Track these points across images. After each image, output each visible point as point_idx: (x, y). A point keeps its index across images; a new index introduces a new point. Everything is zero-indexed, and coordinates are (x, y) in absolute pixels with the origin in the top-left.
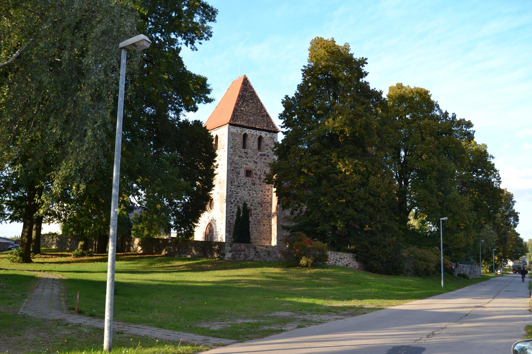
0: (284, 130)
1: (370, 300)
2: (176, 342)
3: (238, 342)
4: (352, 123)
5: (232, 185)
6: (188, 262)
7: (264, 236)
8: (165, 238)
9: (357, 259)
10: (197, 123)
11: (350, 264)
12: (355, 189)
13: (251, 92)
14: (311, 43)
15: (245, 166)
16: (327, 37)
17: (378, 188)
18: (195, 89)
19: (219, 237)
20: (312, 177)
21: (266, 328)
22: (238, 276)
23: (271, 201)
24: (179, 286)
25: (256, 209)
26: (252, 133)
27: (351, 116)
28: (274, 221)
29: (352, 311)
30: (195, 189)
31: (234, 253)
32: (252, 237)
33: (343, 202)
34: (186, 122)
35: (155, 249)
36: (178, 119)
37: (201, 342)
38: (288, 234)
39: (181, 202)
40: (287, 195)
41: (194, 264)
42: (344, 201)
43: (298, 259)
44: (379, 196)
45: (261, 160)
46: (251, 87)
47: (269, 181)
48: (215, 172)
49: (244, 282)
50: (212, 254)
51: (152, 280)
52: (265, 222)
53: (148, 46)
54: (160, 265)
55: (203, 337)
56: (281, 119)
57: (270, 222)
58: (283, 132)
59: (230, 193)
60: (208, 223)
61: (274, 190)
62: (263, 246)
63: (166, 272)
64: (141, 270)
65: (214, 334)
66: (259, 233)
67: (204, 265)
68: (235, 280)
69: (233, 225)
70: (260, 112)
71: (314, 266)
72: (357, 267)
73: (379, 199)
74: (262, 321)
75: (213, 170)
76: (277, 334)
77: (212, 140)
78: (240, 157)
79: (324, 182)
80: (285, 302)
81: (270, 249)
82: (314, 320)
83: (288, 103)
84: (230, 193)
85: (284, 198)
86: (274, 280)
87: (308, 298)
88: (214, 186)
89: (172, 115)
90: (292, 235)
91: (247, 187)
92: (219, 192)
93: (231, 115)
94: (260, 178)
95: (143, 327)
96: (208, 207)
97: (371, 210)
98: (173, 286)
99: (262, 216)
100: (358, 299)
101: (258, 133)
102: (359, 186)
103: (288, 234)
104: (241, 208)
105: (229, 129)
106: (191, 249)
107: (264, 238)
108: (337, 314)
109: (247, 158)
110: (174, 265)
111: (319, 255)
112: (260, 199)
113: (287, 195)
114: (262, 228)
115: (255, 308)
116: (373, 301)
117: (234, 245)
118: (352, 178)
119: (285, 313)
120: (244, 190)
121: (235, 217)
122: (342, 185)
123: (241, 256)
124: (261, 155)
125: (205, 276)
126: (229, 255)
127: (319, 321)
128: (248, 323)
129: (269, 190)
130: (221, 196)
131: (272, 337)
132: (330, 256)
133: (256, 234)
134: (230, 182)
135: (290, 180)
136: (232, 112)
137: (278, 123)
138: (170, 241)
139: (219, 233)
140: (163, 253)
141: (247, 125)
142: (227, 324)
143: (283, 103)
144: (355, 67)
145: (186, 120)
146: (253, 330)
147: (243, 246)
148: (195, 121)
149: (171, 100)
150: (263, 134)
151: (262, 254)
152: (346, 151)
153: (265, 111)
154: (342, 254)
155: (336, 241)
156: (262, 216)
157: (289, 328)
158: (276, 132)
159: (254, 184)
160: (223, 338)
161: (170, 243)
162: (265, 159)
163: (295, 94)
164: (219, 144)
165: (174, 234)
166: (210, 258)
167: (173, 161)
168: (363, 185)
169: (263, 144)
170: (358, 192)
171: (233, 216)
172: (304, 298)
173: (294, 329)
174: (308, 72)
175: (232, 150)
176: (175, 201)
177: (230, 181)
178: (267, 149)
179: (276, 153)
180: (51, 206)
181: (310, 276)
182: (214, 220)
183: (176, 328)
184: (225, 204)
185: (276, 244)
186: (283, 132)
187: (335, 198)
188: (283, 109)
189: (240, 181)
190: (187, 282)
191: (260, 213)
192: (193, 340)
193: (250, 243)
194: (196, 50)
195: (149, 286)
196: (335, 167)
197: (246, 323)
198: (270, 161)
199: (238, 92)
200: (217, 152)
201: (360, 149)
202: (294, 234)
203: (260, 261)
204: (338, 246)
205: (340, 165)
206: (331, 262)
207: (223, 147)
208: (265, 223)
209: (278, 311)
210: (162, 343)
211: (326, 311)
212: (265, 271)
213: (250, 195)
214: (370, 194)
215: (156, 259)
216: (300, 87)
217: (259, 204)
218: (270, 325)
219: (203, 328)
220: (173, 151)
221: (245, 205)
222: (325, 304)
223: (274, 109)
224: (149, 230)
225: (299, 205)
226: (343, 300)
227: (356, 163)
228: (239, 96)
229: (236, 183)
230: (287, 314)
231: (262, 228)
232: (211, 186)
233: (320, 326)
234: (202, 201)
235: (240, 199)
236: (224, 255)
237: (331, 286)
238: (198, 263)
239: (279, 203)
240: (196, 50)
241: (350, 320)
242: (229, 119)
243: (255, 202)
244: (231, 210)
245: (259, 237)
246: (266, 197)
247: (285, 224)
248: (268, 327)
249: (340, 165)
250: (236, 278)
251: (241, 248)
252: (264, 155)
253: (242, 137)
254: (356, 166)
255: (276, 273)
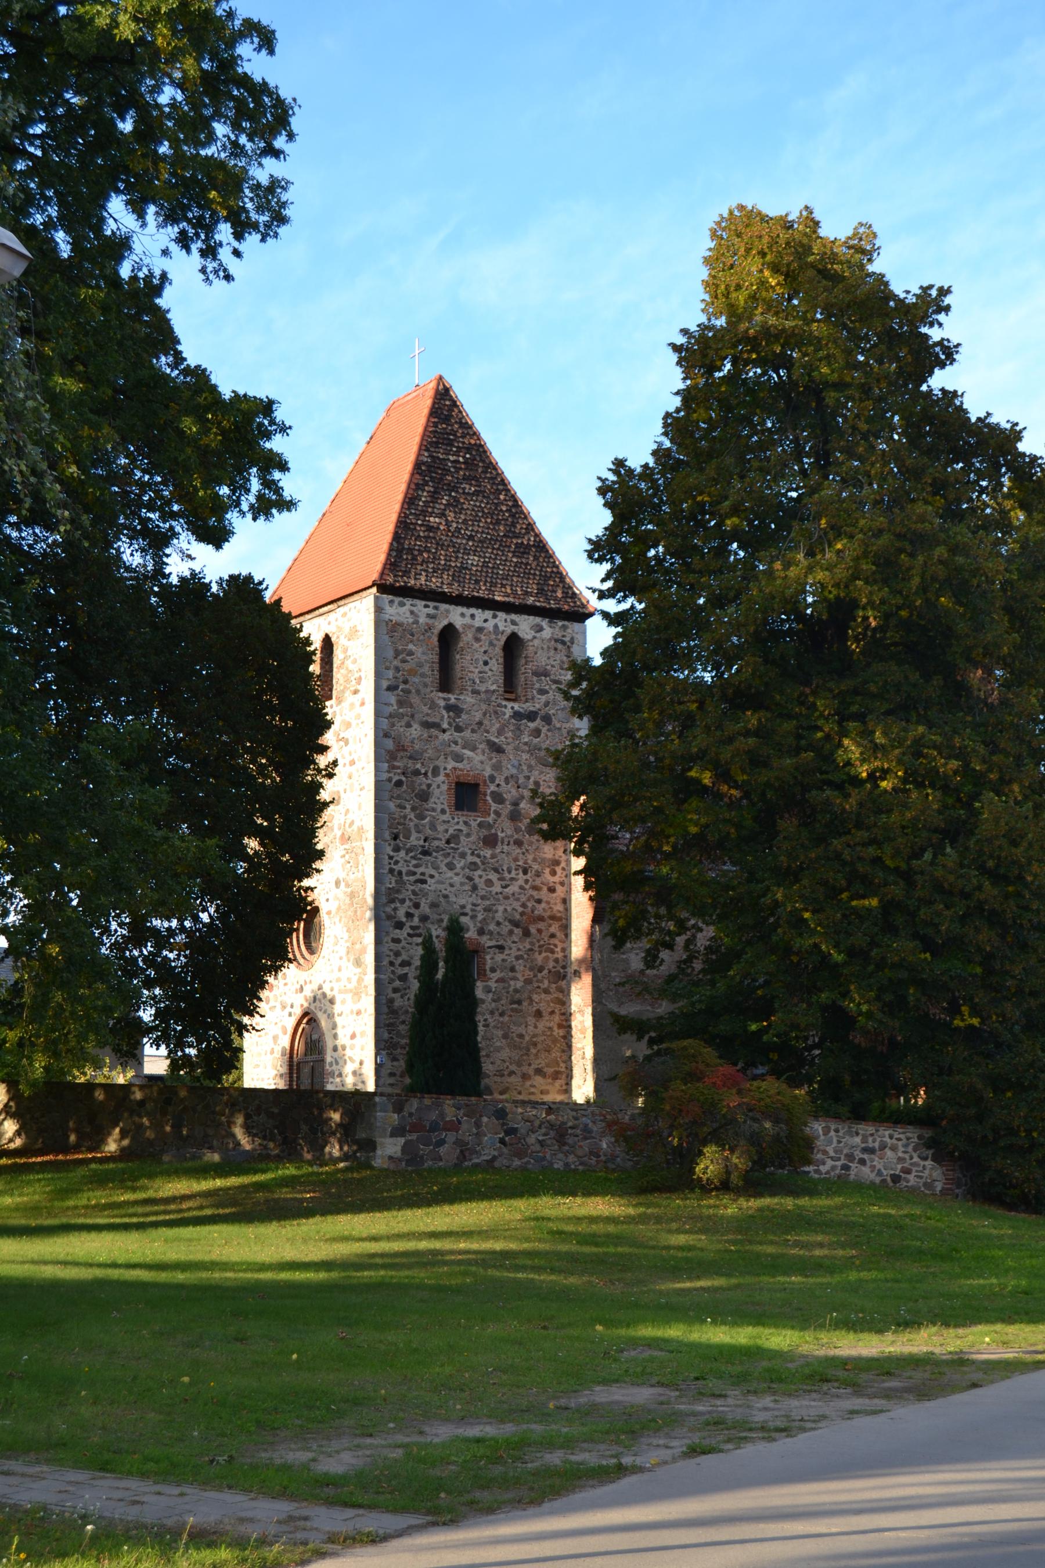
0: (611, 606)
1: (999, 1327)
2: (169, 1531)
3: (434, 1524)
4: (887, 570)
5: (397, 849)
6: (219, 1183)
7: (541, 1062)
8: (121, 1080)
9: (937, 1149)
10: (243, 588)
11: (908, 1171)
12: (917, 854)
13: (468, 450)
14: (714, 234)
15: (451, 764)
16: (780, 203)
17: (1014, 843)
18: (226, 449)
19: (349, 1069)
20: (732, 804)
21: (555, 1458)
22: (434, 1235)
23: (567, 910)
24: (181, 1286)
25: (501, 948)
26: (478, 622)
27: (884, 540)
28: (580, 997)
29: (919, 1376)
30: (241, 867)
31: (414, 1136)
32: (487, 1067)
33: (869, 910)
34: (194, 585)
35: (77, 1131)
36: (159, 571)
37: (272, 1530)
38: (643, 1049)
39: (182, 929)
40: (633, 883)
41: (242, 1188)
42: (874, 902)
43: (688, 1157)
44: (1020, 878)
45: (517, 737)
46: (467, 428)
47: (554, 825)
48: (324, 795)
49: (459, 1263)
50: (318, 1147)
51: (65, 1263)
52: (542, 1001)
53: (17, 269)
54: (100, 1196)
55: (284, 1507)
56: (600, 560)
57: (564, 1002)
58: (606, 615)
59: (391, 882)
60: (298, 1012)
61: (579, 863)
62: (535, 1104)
63: (126, 1227)
64: (19, 1221)
65: (330, 1491)
66: (514, 1046)
67: (285, 1194)
68: (416, 1253)
69: (408, 1018)
70: (511, 534)
71: (753, 1184)
72: (939, 1186)
73: (1019, 895)
74: (538, 1428)
75: (318, 787)
76: (602, 1483)
77: (309, 658)
78: (427, 725)
79: (788, 825)
80: (634, 1343)
81: (566, 1117)
82: (759, 1417)
83: (623, 492)
84: (391, 882)
85: (618, 896)
86: (587, 1249)
87: (734, 1324)
88: (320, 855)
89: (132, 555)
90: (658, 1053)
91: (463, 855)
92: (343, 877)
93: (385, 547)
94: (515, 816)
95: (31, 1470)
96: (296, 943)
97: (986, 937)
98: (155, 1285)
99: (529, 974)
100: (947, 1325)
101: (503, 622)
102: (936, 838)
103: (643, 1049)
104: (439, 945)
105: (378, 610)
106: (230, 1123)
107: (539, 1072)
108: (858, 1389)
109: (459, 729)
110: (161, 1194)
111: (777, 1138)
112: (517, 905)
113: (633, 883)
114: (531, 1028)
115: (504, 1372)
116: (1012, 1329)
117: (414, 1104)
118: (905, 806)
119: (635, 1390)
120: (451, 866)
121: (415, 985)
122: (862, 835)
123: (442, 1150)
124: (517, 715)
125: (291, 1240)
126: (390, 1148)
127: (779, 1424)
128: (478, 1441)
129: (557, 863)
130: (352, 895)
131: (578, 1497)
132: (820, 1143)
133: (505, 1054)
134: (387, 835)
135: (642, 820)
136: (388, 537)
137: (587, 577)
138: (138, 1095)
139: (348, 1053)
140: (112, 1147)
141: (455, 590)
142: (387, 1447)
143: (602, 491)
144: (901, 334)
145: (194, 574)
146: (498, 1470)
147: (450, 1108)
148: (234, 579)
149: (125, 494)
150: (525, 626)
151: (532, 1139)
152: (873, 688)
153: (531, 527)
154: (871, 1129)
155: (847, 1078)
156: (529, 974)
157: (650, 1458)
158: (581, 615)
159: (491, 841)
160: (371, 1507)
161: (142, 1103)
162: (537, 733)
163: (654, 453)
164: (338, 676)
165: (156, 1060)
166: (310, 1163)
167: (142, 758)
168: (954, 832)
169: (525, 671)
170: (932, 863)
171: (403, 978)
172: (714, 1322)
173: (674, 1459)
174: (696, 353)
175: (393, 700)
176: (157, 923)
177: (390, 832)
178: (542, 692)
179: (580, 707)
180: (489, 520)
181: (744, 1225)
182: (327, 996)
183: (169, 1471)
184: (372, 927)
185: (591, 1094)
186: (606, 615)
187: (834, 892)
188: (606, 518)
189: (433, 827)
190: (212, 1266)
191: (520, 966)
192: (242, 1520)
193: (479, 1094)
194: (228, 278)
195: (53, 1288)
196: (828, 758)
197: (467, 1440)
198: (557, 742)
199: (415, 449)
200: (331, 708)
201: (937, 681)
202: (668, 1052)
203: (524, 1168)
204: (858, 1096)
205: (852, 749)
206: (828, 1167)
207: (353, 685)
208: (543, 1006)
209: (605, 1382)
210: (111, 1537)
211: (811, 1377)
212: (547, 1212)
213: (475, 888)
214: (983, 870)
215: (82, 1171)
216: (672, 424)
217: (516, 924)
218: (569, 1444)
219: (286, 1468)
220: (139, 707)
221: (455, 929)
222: (805, 1349)
223: (569, 520)
224: (53, 1050)
225: (682, 926)
226: (880, 1331)
227: (918, 742)
228: (418, 465)
229: (415, 840)
230: (642, 1395)
231: (531, 1028)
232: (308, 857)
233: (784, 1445)
234: (271, 922)
235: (434, 905)
236: (370, 1145)
237: (831, 1271)
238: (259, 1186)
239: (597, 919)
240: (228, 278)
241: (913, 1418)
242: (379, 567)
243: (499, 916)
244: (397, 954)
245: (519, 1064)
246: (544, 894)
247: (629, 1009)
248: (560, 1453)
249: (852, 749)
250: (423, 1245)
251: (442, 1115)
252: (531, 716)
253: (435, 640)
254: (918, 755)
255: (593, 1220)
